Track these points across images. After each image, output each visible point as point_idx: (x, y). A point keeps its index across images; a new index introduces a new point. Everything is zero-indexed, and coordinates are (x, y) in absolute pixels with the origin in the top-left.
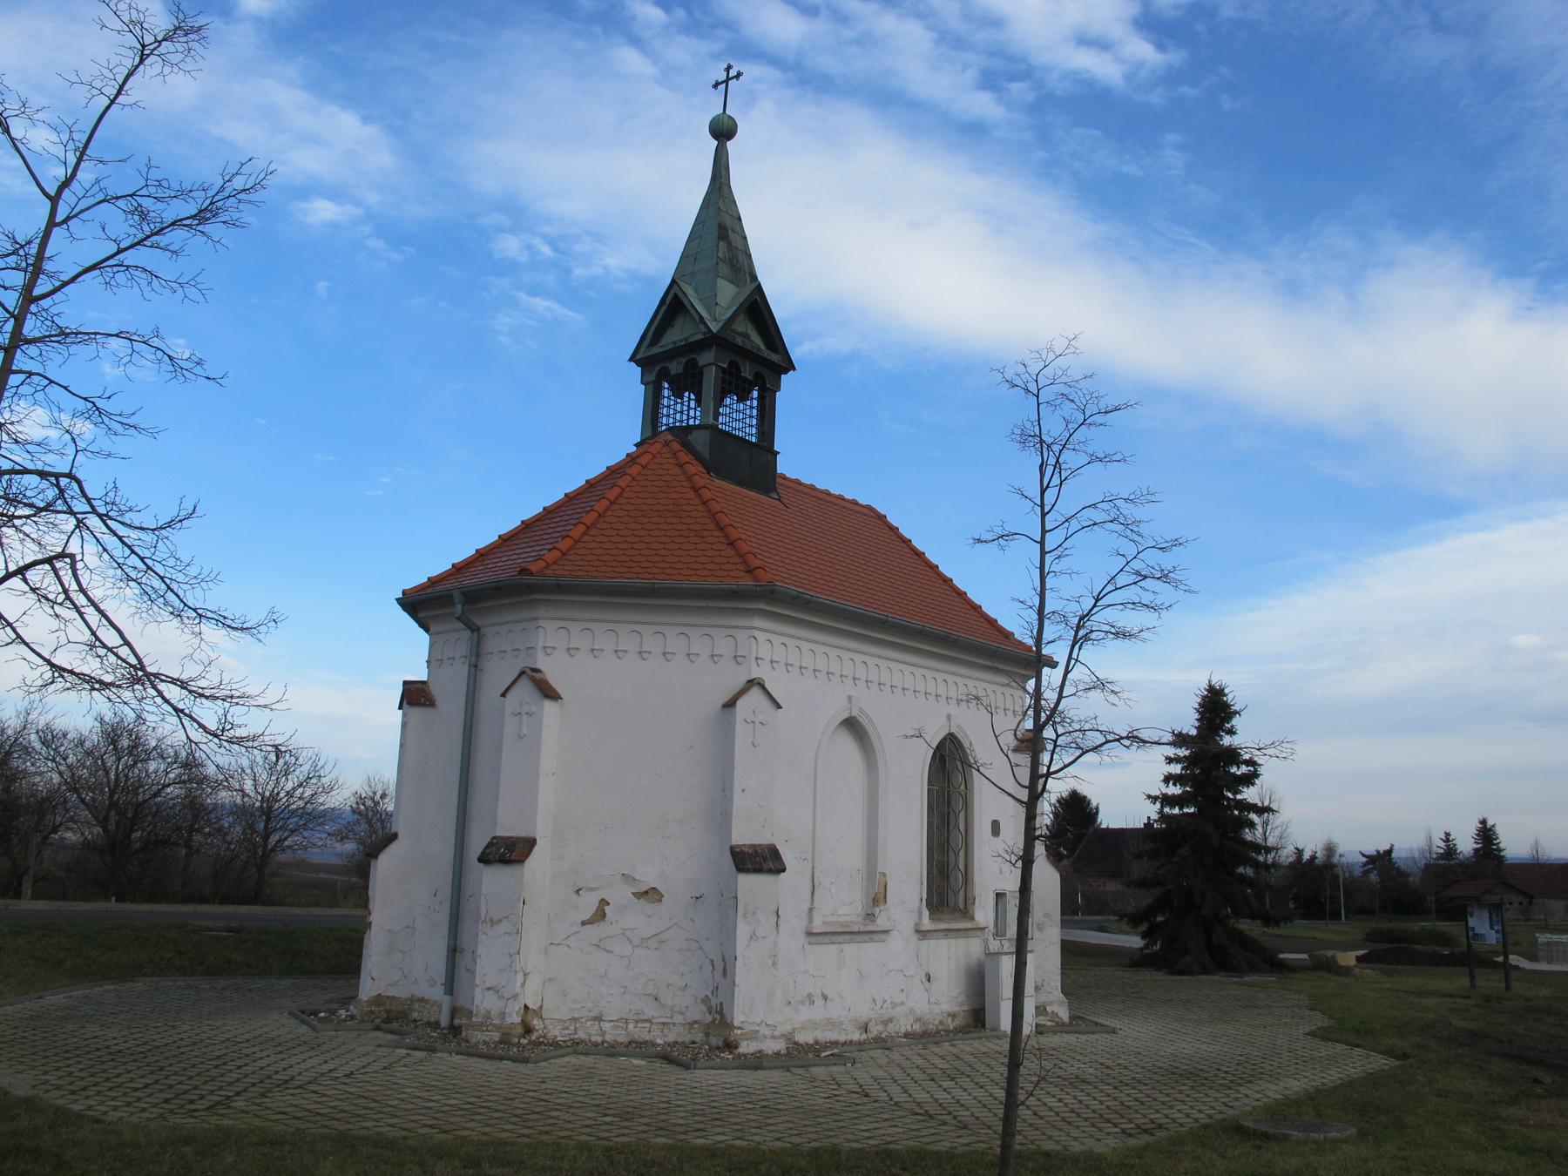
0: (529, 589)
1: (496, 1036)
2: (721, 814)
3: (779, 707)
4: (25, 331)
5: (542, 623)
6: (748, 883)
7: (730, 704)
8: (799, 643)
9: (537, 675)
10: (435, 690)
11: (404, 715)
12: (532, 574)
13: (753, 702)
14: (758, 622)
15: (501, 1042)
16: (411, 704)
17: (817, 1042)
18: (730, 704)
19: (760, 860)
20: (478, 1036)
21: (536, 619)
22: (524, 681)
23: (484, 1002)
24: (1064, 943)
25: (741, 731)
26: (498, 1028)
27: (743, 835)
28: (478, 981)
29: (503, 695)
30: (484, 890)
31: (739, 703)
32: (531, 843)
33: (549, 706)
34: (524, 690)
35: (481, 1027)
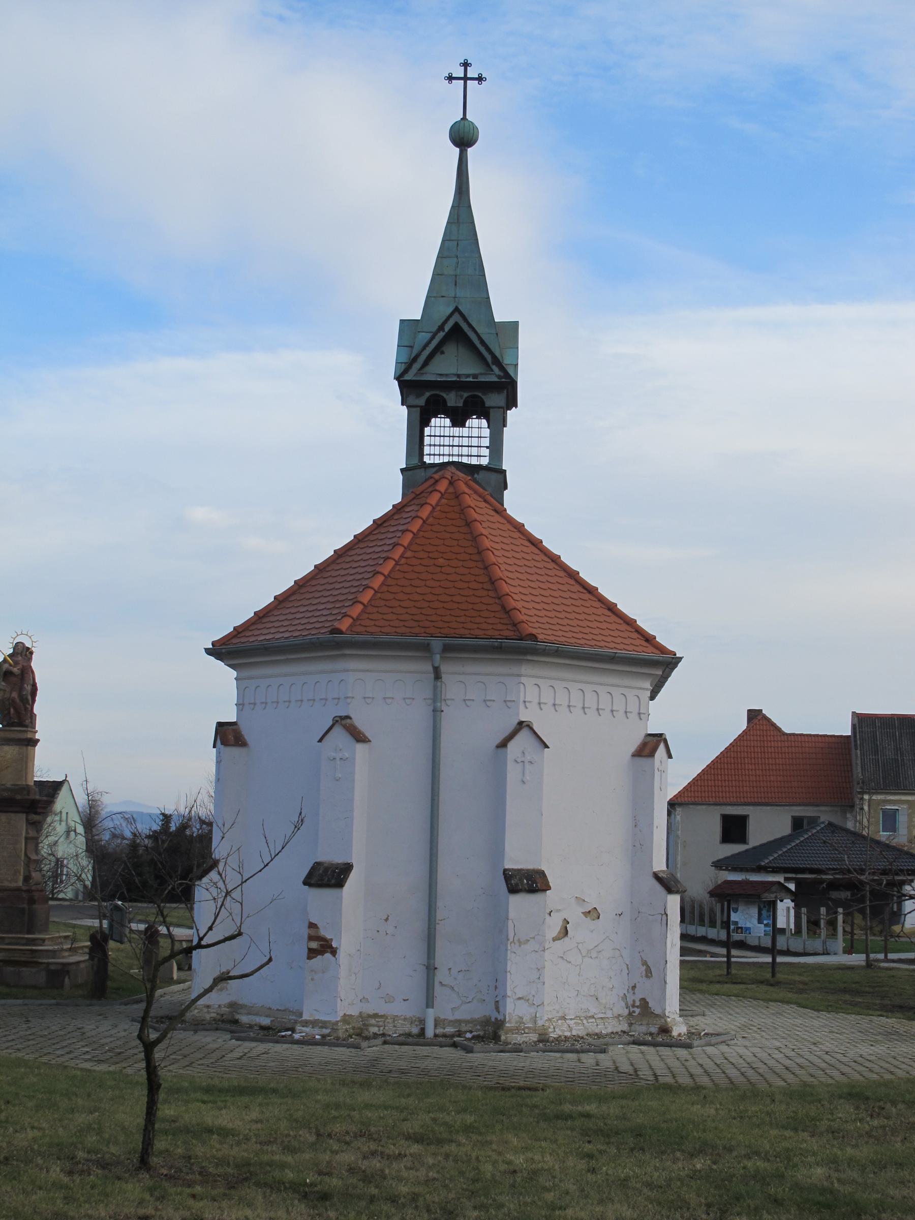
0: (339, 645)
1: (534, 1037)
2: (497, 846)
3: (547, 747)
4: (485, 461)
5: (523, 680)
6: (519, 904)
7: (503, 744)
8: (610, 689)
9: (348, 721)
10: (246, 732)
11: (219, 754)
12: (341, 632)
13: (523, 740)
14: (353, 664)
15: (540, 1041)
16: (225, 743)
17: (196, 1032)
18: (503, 744)
19: (530, 882)
20: (519, 1039)
21: (519, 676)
22: (338, 730)
23: (514, 1011)
24: (682, 962)
25: (513, 773)
26: (535, 1030)
27: (516, 860)
28: (509, 993)
29: (320, 741)
30: (512, 915)
31: (511, 745)
32: (347, 868)
33: (360, 747)
34: (339, 736)
35: (517, 1030)
